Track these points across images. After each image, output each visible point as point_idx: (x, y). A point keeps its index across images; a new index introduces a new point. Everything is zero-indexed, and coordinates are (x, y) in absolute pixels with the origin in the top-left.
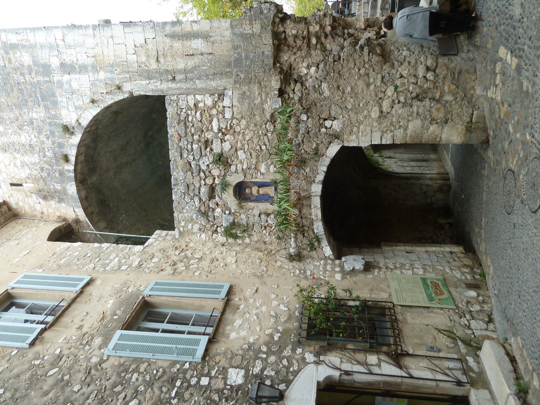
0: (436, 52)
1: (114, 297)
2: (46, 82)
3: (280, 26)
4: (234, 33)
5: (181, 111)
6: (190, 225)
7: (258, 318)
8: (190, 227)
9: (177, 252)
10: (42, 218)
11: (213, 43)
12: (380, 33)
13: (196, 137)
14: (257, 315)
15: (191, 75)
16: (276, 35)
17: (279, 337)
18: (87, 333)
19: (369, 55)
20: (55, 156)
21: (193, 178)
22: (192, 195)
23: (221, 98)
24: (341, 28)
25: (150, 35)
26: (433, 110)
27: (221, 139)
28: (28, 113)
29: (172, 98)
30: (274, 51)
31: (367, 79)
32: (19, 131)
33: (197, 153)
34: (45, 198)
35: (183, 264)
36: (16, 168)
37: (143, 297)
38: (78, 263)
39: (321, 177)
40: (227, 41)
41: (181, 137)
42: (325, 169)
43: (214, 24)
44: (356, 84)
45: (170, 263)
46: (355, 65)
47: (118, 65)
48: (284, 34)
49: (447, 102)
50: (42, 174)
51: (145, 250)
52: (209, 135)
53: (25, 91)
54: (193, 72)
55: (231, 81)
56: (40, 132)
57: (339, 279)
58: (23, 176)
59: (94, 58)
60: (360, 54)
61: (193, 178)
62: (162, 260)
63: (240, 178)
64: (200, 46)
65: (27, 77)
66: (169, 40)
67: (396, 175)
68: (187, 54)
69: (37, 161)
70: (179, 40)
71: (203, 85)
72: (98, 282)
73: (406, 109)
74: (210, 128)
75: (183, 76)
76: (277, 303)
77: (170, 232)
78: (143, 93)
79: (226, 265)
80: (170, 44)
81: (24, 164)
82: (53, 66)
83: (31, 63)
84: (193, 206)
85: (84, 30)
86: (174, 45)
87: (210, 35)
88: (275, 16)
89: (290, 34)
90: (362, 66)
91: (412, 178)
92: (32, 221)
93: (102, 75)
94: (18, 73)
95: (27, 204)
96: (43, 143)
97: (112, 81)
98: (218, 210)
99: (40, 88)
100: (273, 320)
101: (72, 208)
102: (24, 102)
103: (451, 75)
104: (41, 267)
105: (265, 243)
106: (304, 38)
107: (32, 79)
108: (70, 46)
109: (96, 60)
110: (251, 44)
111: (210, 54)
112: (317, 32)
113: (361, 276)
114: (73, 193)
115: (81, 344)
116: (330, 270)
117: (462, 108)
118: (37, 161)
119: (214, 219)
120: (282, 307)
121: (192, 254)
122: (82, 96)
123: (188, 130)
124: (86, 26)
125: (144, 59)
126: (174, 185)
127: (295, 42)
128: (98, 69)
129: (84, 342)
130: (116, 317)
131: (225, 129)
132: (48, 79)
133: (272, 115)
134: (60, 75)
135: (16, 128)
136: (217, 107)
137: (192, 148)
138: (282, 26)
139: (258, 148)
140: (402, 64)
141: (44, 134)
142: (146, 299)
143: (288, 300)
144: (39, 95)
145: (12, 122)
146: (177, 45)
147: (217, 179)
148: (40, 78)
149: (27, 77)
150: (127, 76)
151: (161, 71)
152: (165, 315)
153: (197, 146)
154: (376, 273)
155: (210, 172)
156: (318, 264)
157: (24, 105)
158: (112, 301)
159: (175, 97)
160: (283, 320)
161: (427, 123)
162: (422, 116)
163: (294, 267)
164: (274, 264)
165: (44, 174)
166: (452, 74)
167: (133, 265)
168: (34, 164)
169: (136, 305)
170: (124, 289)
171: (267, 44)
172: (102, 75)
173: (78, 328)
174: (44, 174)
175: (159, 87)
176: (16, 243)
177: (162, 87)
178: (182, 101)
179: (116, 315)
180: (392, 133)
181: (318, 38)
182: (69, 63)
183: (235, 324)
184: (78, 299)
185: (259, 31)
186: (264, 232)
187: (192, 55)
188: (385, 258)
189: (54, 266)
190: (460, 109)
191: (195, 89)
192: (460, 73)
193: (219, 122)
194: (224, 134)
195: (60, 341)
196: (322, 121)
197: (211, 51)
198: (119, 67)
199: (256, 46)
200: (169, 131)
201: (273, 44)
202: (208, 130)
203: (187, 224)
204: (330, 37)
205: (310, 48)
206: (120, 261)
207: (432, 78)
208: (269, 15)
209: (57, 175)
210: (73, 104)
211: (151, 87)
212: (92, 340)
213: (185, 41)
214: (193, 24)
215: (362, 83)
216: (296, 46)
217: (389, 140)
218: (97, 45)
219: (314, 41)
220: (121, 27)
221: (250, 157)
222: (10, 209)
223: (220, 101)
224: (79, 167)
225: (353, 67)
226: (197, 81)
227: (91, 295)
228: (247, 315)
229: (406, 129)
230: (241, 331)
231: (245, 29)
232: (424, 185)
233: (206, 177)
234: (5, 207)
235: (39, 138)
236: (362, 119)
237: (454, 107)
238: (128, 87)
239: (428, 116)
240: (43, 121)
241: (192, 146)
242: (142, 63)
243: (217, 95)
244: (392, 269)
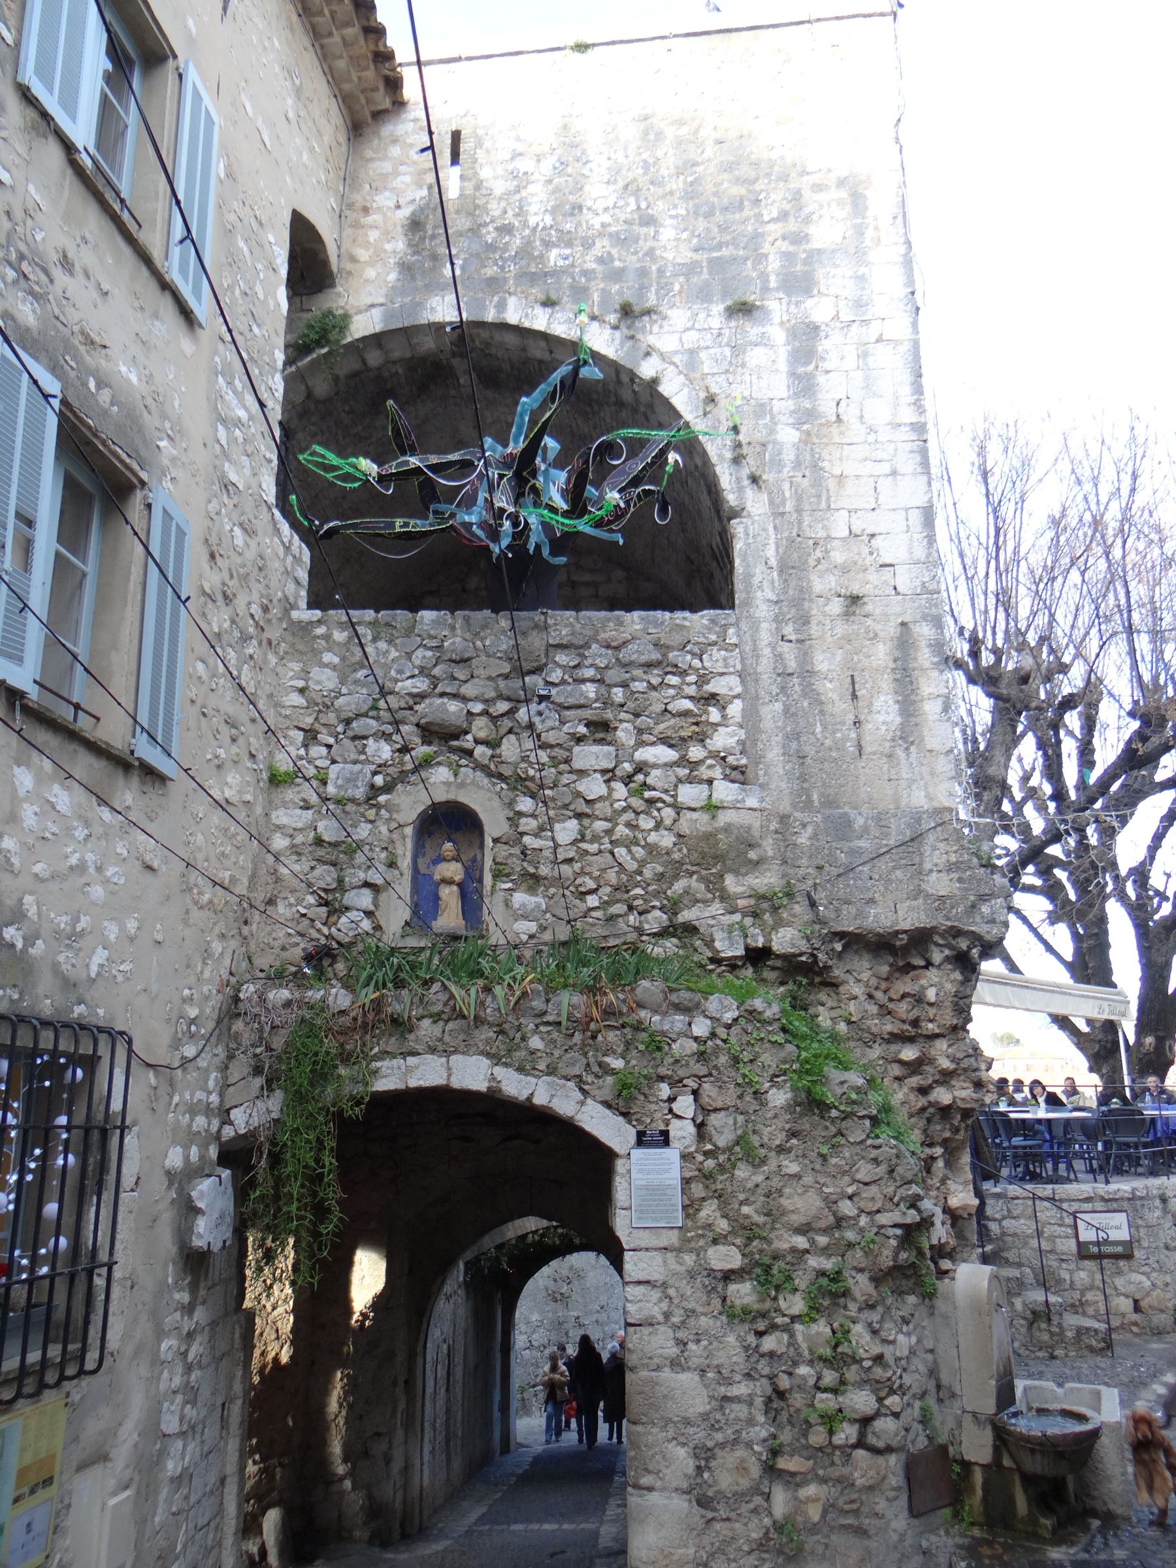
0: (913, 1442)
1: (145, 390)
2: (764, 277)
3: (947, 952)
4: (920, 818)
5: (693, 654)
6: (336, 660)
7: (71, 868)
8: (328, 657)
9: (255, 609)
10: (350, 206)
11: (890, 756)
12: (943, 1257)
13: (618, 694)
14: (81, 868)
15: (797, 688)
16: (921, 939)
17: (13, 946)
18: (51, 281)
19: (895, 1226)
20: (546, 274)
21: (490, 678)
22: (437, 671)
23: (735, 775)
24: (947, 1134)
25: (905, 580)
26: (740, 1453)
27: (612, 770)
28: (676, 217)
29: (731, 631)
30: (879, 935)
31: (823, 1224)
32: (621, 184)
33: (570, 695)
34: (415, 225)
35: (226, 625)
36: (508, 156)
37: (143, 483)
38: (237, 292)
39: (514, 1085)
40: (896, 799)
41: (617, 648)
42: (540, 1100)
43: (942, 760)
44: (807, 1188)
45: (231, 584)
46: (866, 1184)
47: (817, 483)
48: (923, 963)
49: (768, 1497)
50: (491, 228)
51: (265, 509)
52: (625, 733)
53: (737, 216)
54: (805, 694)
55: (785, 806)
56: (620, 240)
57: (168, 1163)
58: (485, 173)
59: (834, 418)
60: (896, 1199)
61: (490, 678)
62: (239, 560)
63: (494, 823)
64: (881, 718)
65: (775, 229)
66: (892, 630)
67: (421, 1343)
68: (857, 679)
69: (532, 221)
70: (895, 661)
71: (767, 724)
72: (186, 345)
73: (740, 1359)
74: (645, 737)
75: (792, 665)
76: (112, 937)
77: (304, 593)
78: (738, 546)
79: (219, 767)
80: (881, 634)
81: (521, 180)
82: (809, 303)
83: (815, 244)
84: (400, 672)
85: (912, 399)
86: (881, 646)
87: (913, 749)
88: (976, 938)
89: (923, 982)
90: (862, 1204)
91: (411, 1402)
92: (342, 174)
93: (788, 435)
94: (787, 207)
95: (395, 168)
96: (588, 244)
97: (772, 461)
98: (385, 751)
99: (747, 259)
100: (63, 921)
101: (382, 300)
102: (706, 208)
103: (852, 1502)
104: (229, 175)
105: (271, 902)
106: (915, 1023)
107: (771, 239)
108: (865, 355)
109: (828, 424)
110: (894, 868)
111: (860, 748)
112: (932, 1061)
113: (167, 1245)
114: (432, 309)
115: (22, 257)
116: (194, 1128)
117: (749, 1553)
118: (532, 221)
119: (354, 738)
120: (100, 957)
121: (251, 657)
122: (727, 372)
123: (638, 672)
124: (920, 407)
125: (838, 557)
126: (467, 620)
127: (904, 996)
128: (805, 427)
129: (25, 266)
130: (92, 385)
131: (645, 784)
132: (773, 284)
133: (690, 929)
134: (785, 318)
135: (631, 176)
136: (709, 762)
137: (584, 681)
138: (947, 959)
139: (592, 885)
140: (875, 1332)
141: (614, 252)
142: (139, 494)
143: (120, 978)
144: (725, 252)
145: (646, 166)
146: (881, 654)
147: (489, 752)
148: (774, 264)
149: (775, 229)
150: (789, 507)
151: (806, 604)
152: (82, 555)
153: (592, 695)
154: (177, 1296)
155: (510, 731)
156: (211, 1084)
157: (697, 206)
158: (134, 378)
159: (734, 640)
160: (61, 958)
161: (698, 1434)
162: (718, 1416)
163: (207, 998)
164: (217, 930)
165: (490, 234)
166: (855, 1506)
167: (227, 465)
168: (521, 208)
169: (124, 456)
170: (168, 425)
171: (896, 913)
172: (788, 435)
173: (65, 256)
174: (490, 234)
175: (759, 594)
176: (291, 115)
177: (759, 602)
178: (725, 659)
179: (99, 386)
180: (661, 1318)
181: (914, 1067)
182: (820, 349)
183: (56, 788)
184: (145, 272)
185: (931, 891)
186: (311, 899)
187: (854, 696)
188: (213, 1324)
189: (232, 217)
190: (746, 1548)
191: (757, 697)
192: (861, 1532)
193: (666, 765)
194: (628, 780)
195: (32, 188)
196: (692, 1083)
197: (868, 749)
198: (813, 486)
199: (890, 881)
200: (636, 614)
201: (897, 932)
202: (640, 731)
203: (336, 649)
204: (922, 1101)
205: (888, 1042)
206: (238, 423)
207: (839, 1439)
208: (978, 919)
209: (490, 271)
210: (702, 344)
211: (759, 572)
212: (31, 293)
213: (892, 677)
214: (940, 701)
215: (814, 1211)
216: (891, 1000)
217: (641, 1309)
218: (872, 430)
219: (909, 1053)
220: (922, 501)
221: (560, 858)
222: (379, 115)
223: (728, 771)
224: (511, 339)
225: (859, 1176)
226: (778, 706)
227: (156, 316)
228: (80, 833)
229: (676, 1364)
230: (36, 808)
231: (934, 848)
232: (390, 1447)
233: (494, 719)
234: (387, 103)
235: (601, 235)
236: (703, 1214)
237: (752, 1525)
238: (755, 504)
239: (719, 1437)
240: (651, 253)
241: (592, 681)
242: (827, 551)
243: (744, 761)
244: (185, 1354)
